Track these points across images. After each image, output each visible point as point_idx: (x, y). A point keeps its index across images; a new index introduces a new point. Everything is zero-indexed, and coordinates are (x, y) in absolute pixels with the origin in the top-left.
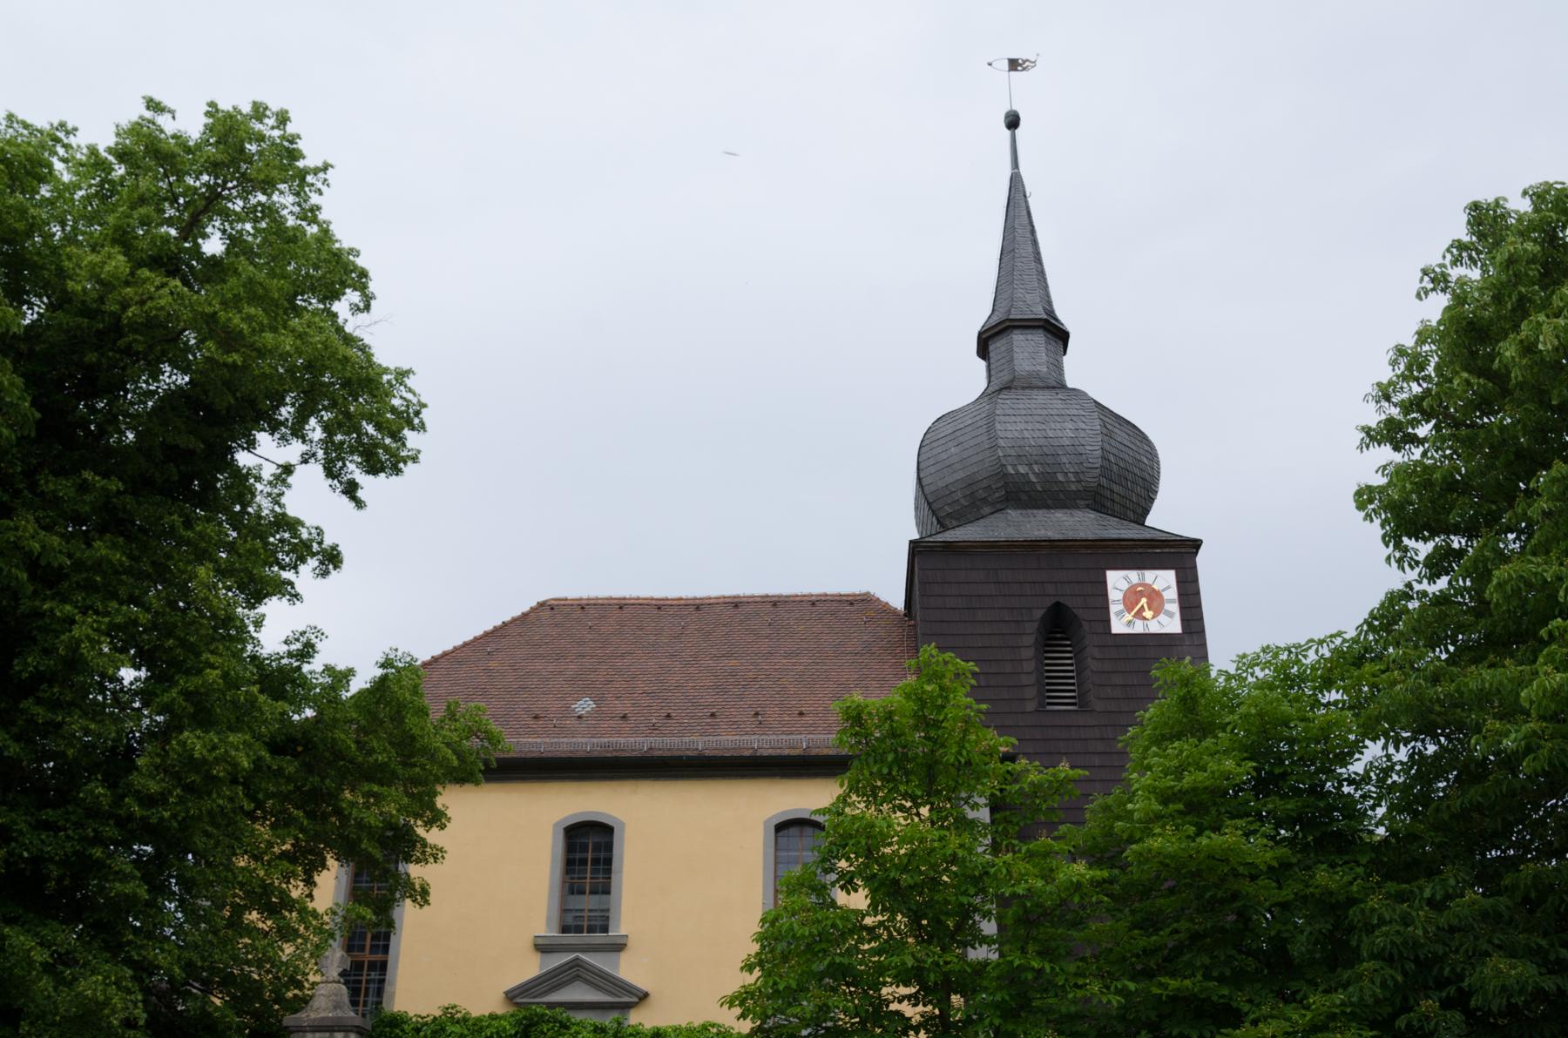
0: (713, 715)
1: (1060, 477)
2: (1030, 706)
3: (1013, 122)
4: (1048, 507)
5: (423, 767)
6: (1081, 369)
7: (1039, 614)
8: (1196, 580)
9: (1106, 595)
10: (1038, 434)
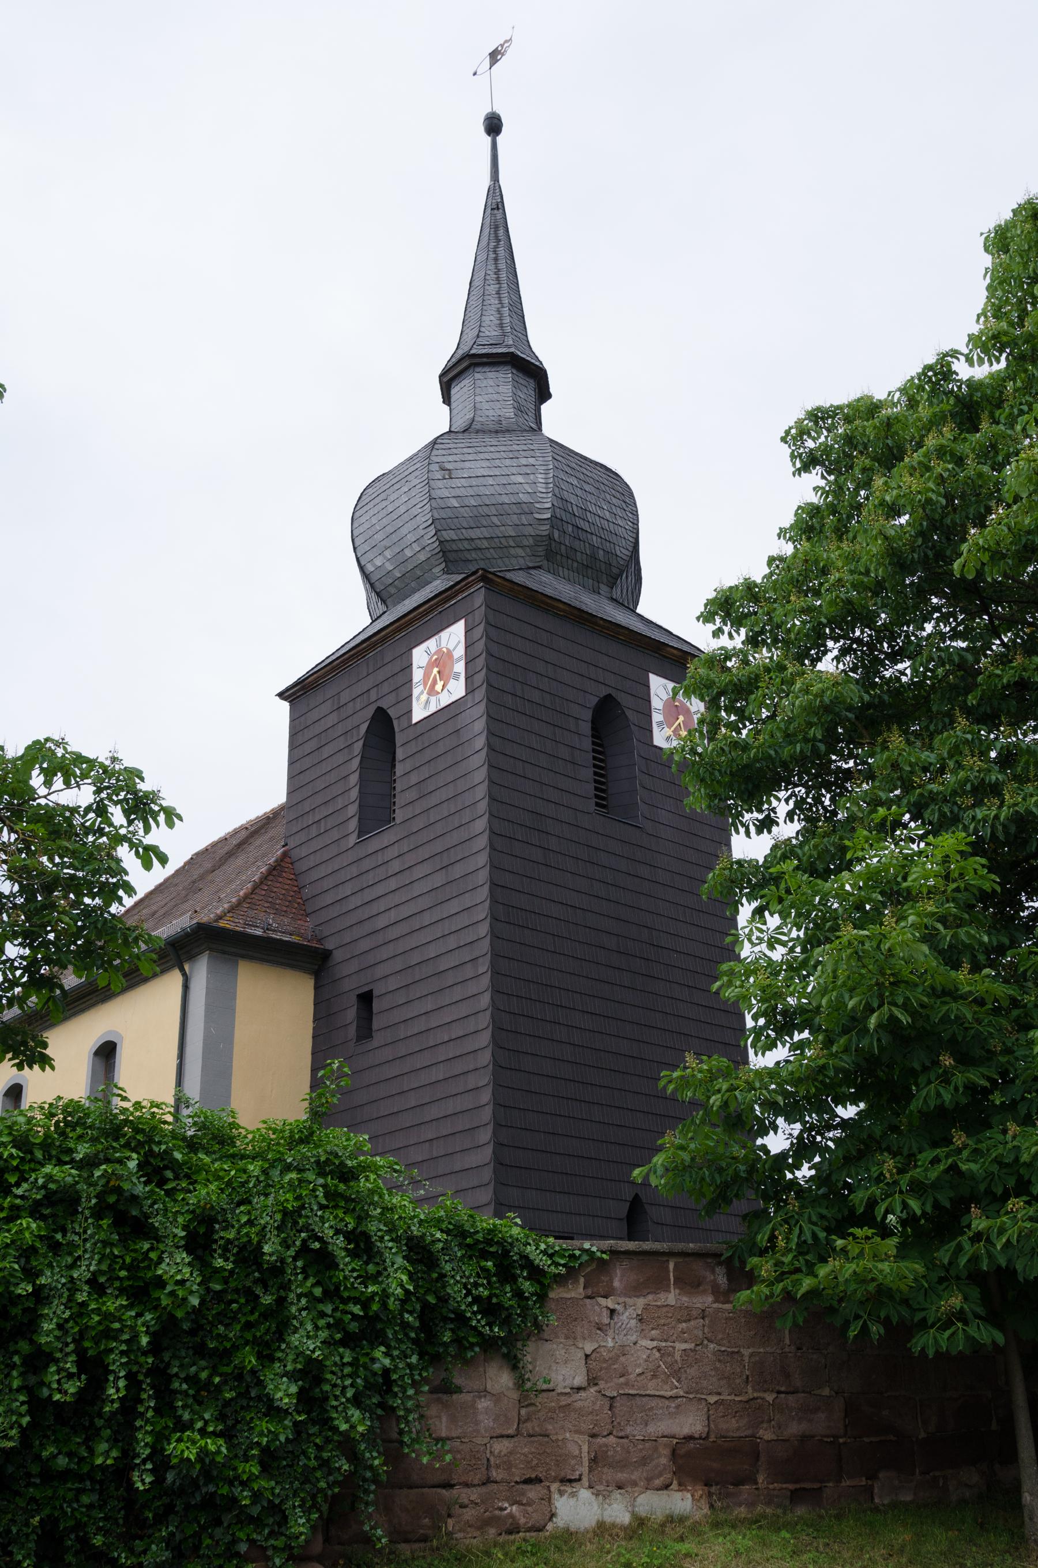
3: (493, 126)
5: (222, 1238)
7: (594, 700)
9: (649, 701)
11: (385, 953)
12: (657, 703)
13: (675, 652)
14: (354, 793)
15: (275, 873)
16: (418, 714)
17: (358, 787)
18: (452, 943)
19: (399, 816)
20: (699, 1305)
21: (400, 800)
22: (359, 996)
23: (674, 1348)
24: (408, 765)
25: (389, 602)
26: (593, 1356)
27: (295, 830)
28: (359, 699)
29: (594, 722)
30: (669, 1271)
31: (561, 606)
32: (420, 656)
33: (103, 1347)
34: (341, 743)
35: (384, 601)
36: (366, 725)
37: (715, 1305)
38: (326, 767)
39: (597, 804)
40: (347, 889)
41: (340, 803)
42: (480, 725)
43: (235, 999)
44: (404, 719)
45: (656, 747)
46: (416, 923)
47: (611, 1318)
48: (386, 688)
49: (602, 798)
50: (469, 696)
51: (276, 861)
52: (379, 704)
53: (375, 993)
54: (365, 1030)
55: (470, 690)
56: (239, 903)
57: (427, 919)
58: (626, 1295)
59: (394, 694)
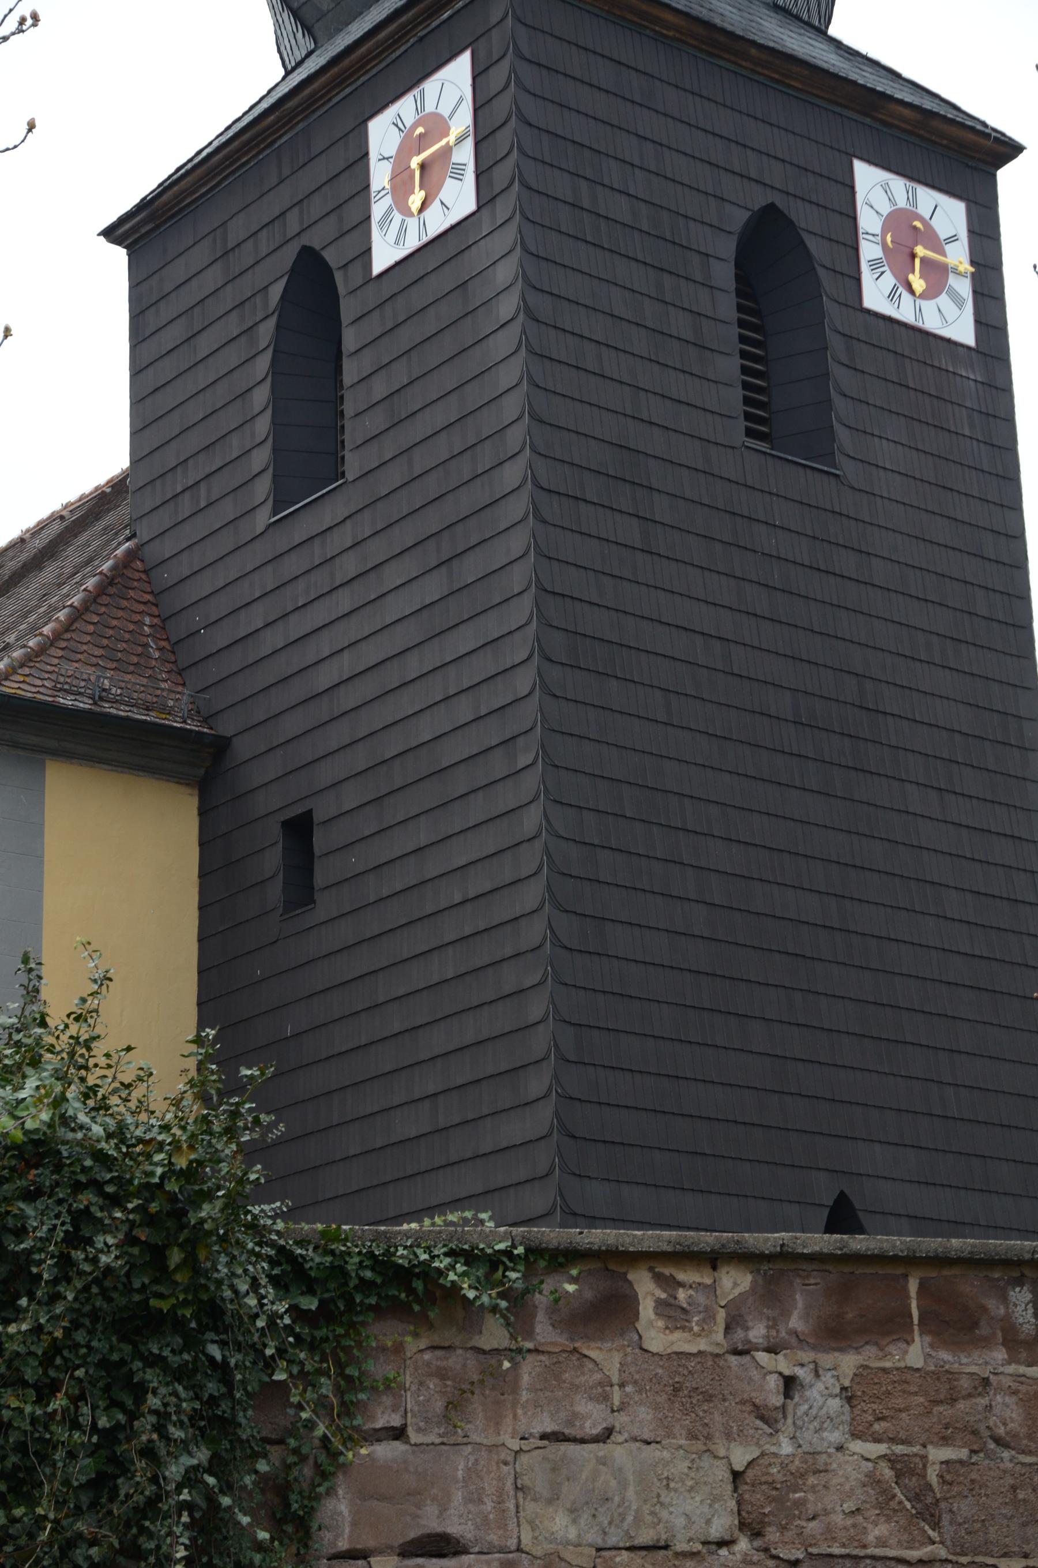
7: (740, 218)
11: (338, 735)
12: (869, 221)
13: (906, 112)
14: (263, 425)
15: (112, 590)
16: (384, 254)
17: (269, 413)
18: (463, 711)
19: (353, 465)
20: (973, 1369)
21: (352, 435)
22: (286, 824)
23: (924, 1458)
24: (367, 362)
25: (317, 28)
26: (750, 1474)
27: (148, 506)
28: (264, 232)
29: (740, 263)
30: (908, 1297)
31: (670, 17)
32: (383, 134)
34: (233, 326)
35: (308, 30)
36: (281, 285)
37: (1011, 1369)
38: (203, 376)
39: (750, 433)
40: (256, 617)
41: (235, 446)
42: (505, 272)
43: (40, 834)
44: (356, 268)
45: (869, 312)
46: (392, 676)
47: (788, 1394)
48: (317, 207)
49: (761, 421)
50: (485, 212)
51: (113, 568)
52: (305, 240)
53: (318, 817)
54: (301, 889)
55: (485, 198)
56: (42, 651)
57: (413, 665)
58: (814, 1348)
59: (333, 218)
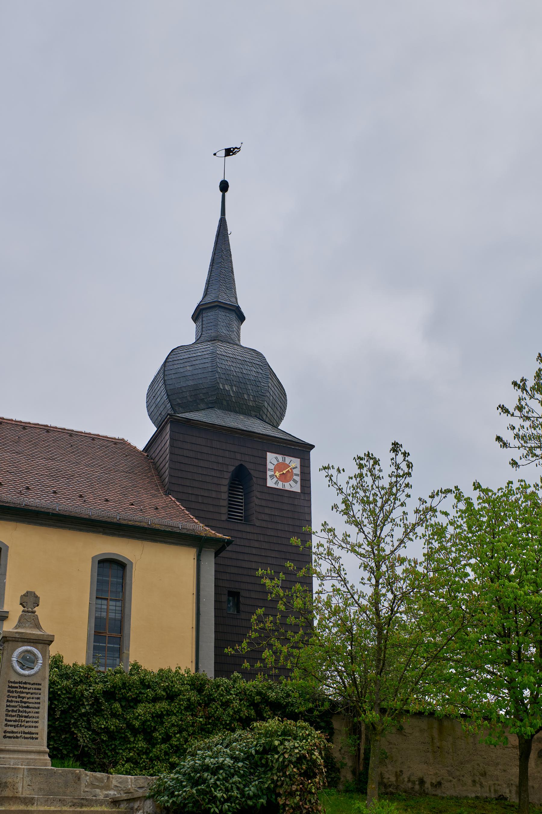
0: (55, 492)
1: (246, 397)
2: (224, 517)
3: (224, 186)
4: (236, 412)
6: (249, 336)
7: (232, 469)
8: (309, 467)
10: (237, 370)
33: (198, 775)
